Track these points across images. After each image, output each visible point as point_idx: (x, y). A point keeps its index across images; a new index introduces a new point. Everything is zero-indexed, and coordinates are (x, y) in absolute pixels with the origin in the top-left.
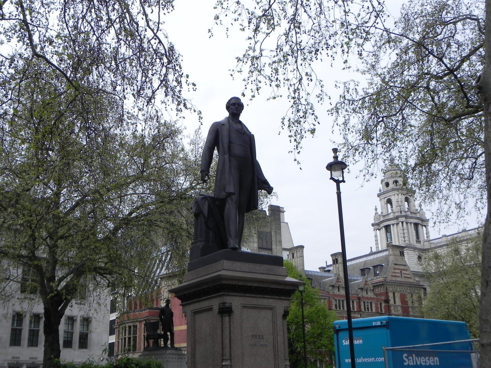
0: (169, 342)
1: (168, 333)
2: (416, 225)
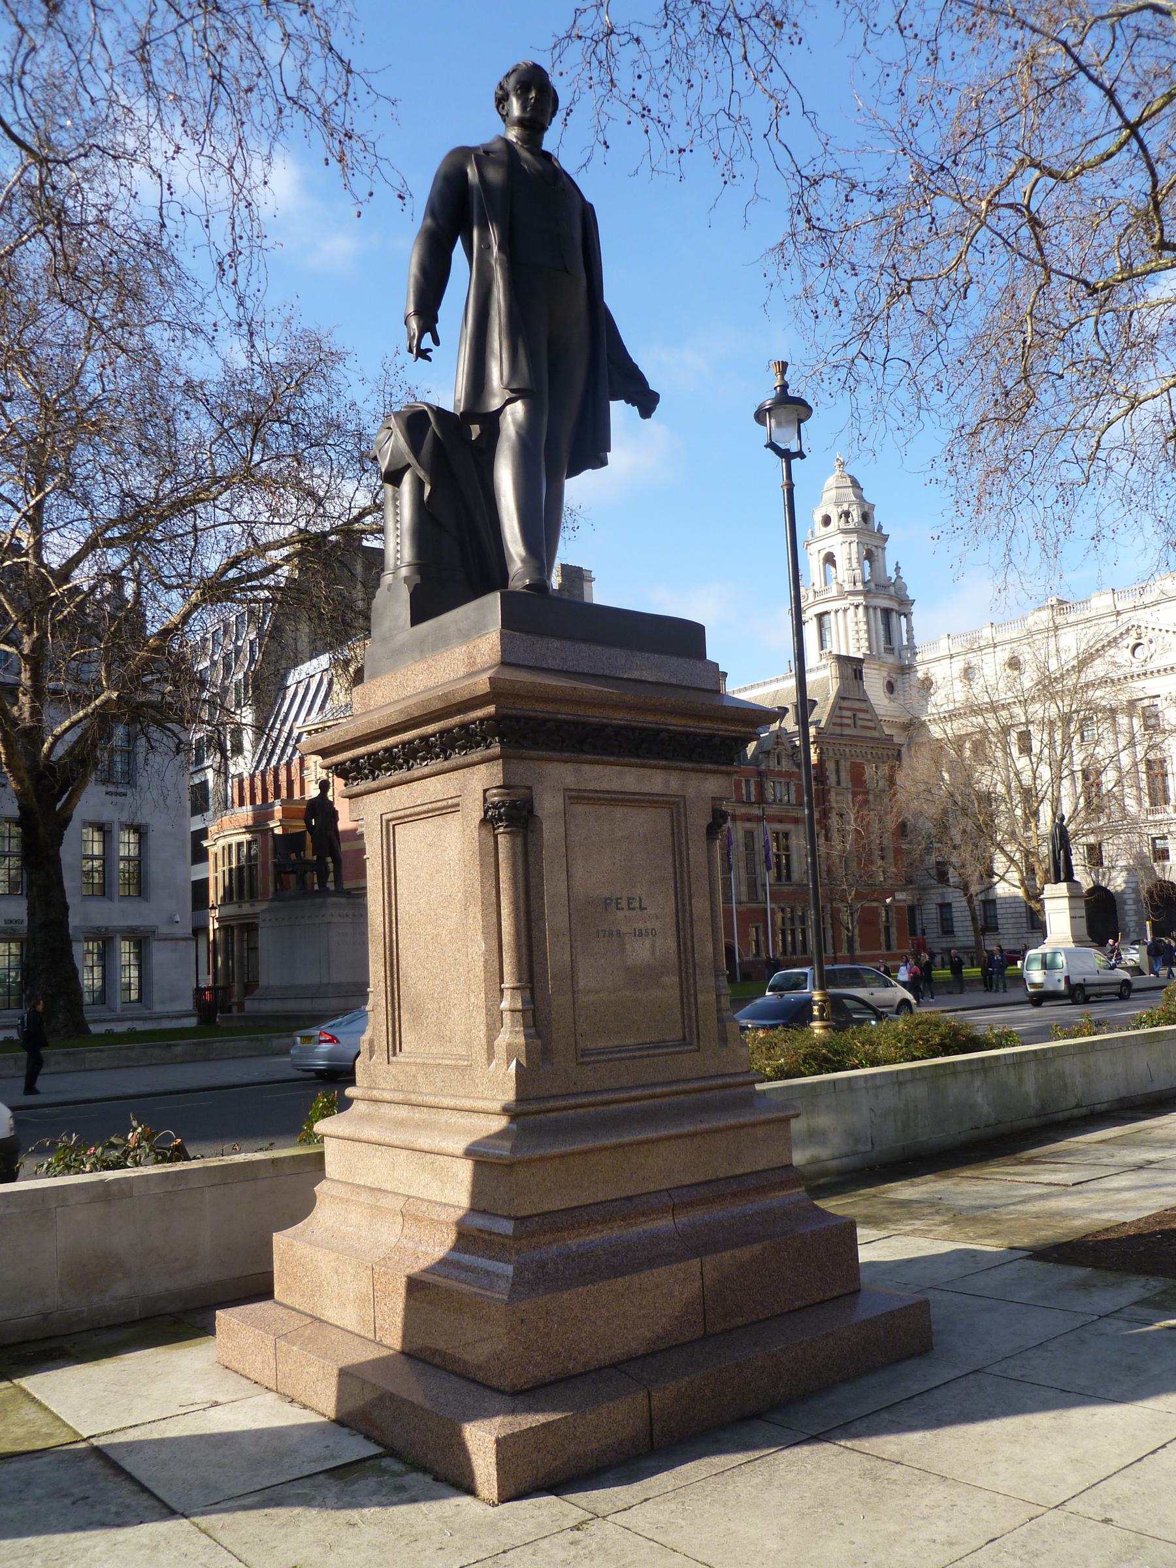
0: (331, 877)
1: (329, 859)
2: (887, 612)
